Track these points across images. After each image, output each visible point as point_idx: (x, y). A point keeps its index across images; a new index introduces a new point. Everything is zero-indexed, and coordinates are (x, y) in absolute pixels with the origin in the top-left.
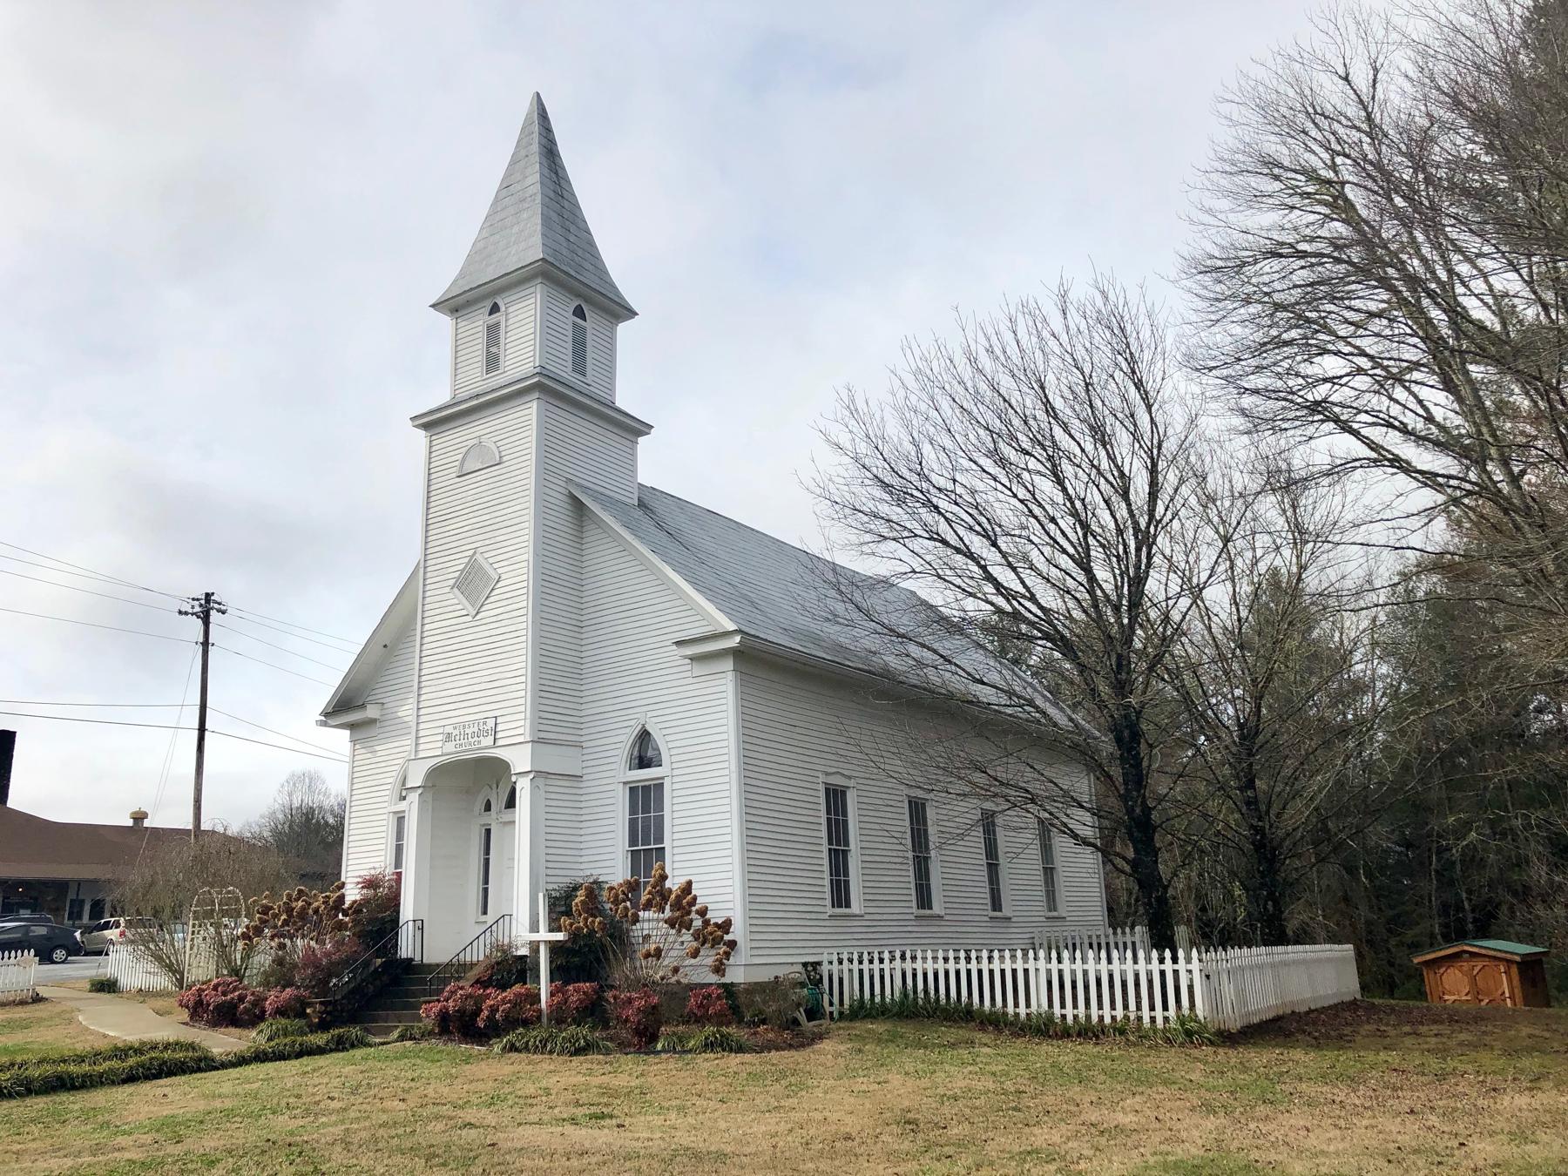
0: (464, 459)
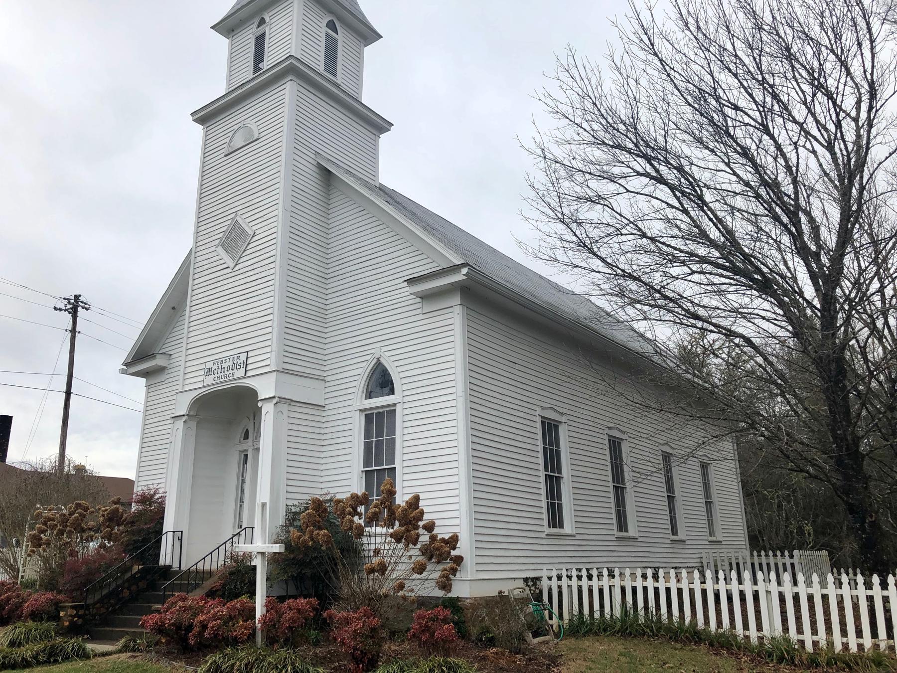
0: (231, 140)
